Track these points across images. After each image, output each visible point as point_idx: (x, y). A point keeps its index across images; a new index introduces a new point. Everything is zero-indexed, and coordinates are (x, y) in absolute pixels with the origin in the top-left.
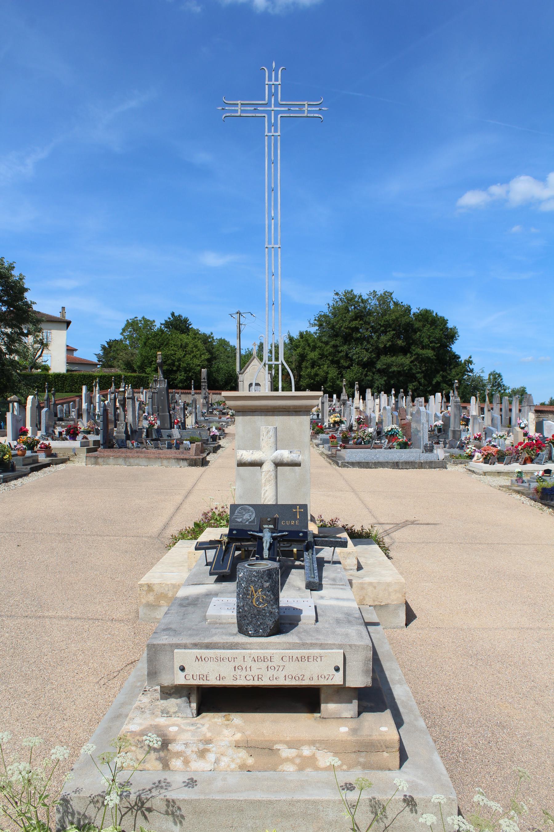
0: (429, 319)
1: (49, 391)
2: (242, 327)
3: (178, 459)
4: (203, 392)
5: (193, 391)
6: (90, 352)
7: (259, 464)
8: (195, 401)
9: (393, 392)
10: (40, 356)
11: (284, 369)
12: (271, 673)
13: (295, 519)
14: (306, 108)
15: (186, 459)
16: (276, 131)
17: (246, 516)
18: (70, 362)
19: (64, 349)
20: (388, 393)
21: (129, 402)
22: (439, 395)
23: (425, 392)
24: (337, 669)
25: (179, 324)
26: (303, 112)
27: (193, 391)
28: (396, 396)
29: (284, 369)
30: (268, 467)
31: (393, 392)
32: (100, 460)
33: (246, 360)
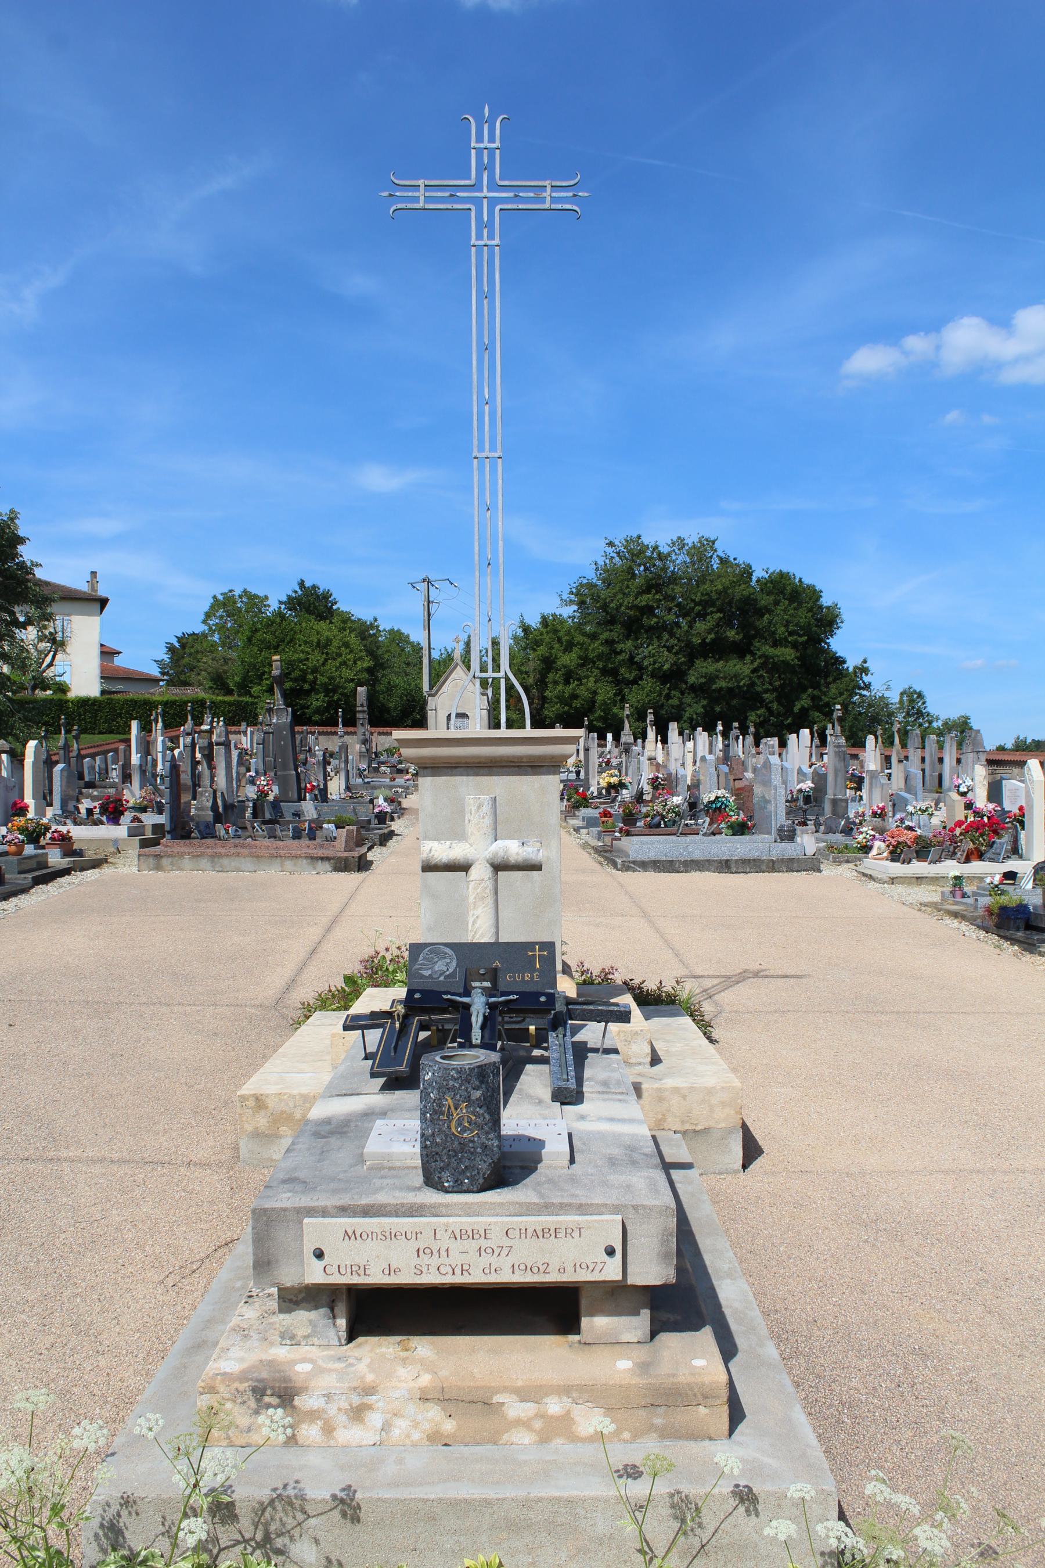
0: (787, 591)
1: (68, 732)
2: (433, 607)
3: (314, 859)
4: (360, 730)
5: (341, 729)
6: (145, 657)
7: (462, 867)
8: (344, 748)
9: (720, 728)
10: (51, 665)
11: (510, 687)
12: (486, 1259)
13: (533, 970)
14: (547, 194)
15: (328, 859)
16: (491, 237)
17: (440, 966)
18: (108, 676)
19: (97, 651)
20: (710, 729)
21: (219, 752)
22: (805, 732)
23: (780, 728)
24: (610, 1252)
25: (313, 603)
26: (543, 200)
27: (341, 729)
28: (725, 735)
29: (510, 687)
30: (480, 872)
31: (720, 728)
32: (165, 862)
33: (441, 669)
